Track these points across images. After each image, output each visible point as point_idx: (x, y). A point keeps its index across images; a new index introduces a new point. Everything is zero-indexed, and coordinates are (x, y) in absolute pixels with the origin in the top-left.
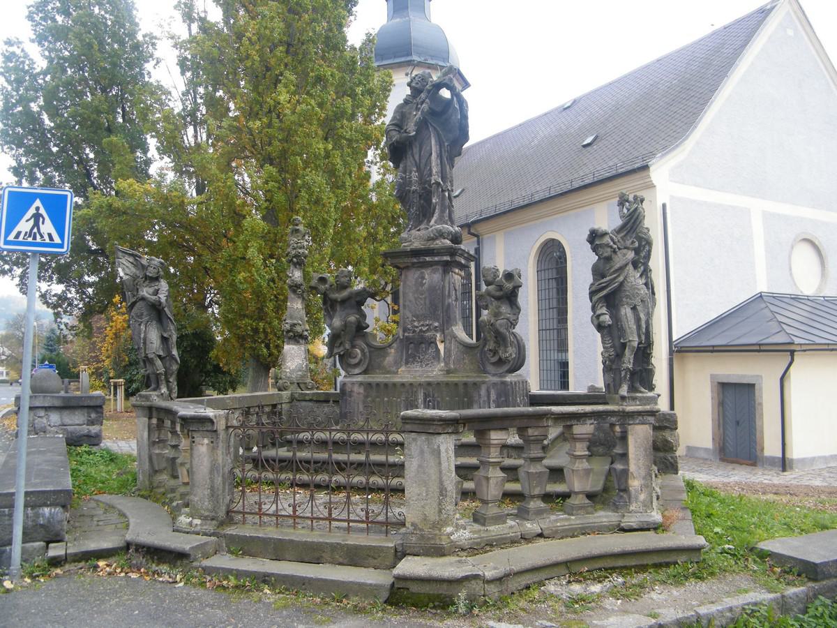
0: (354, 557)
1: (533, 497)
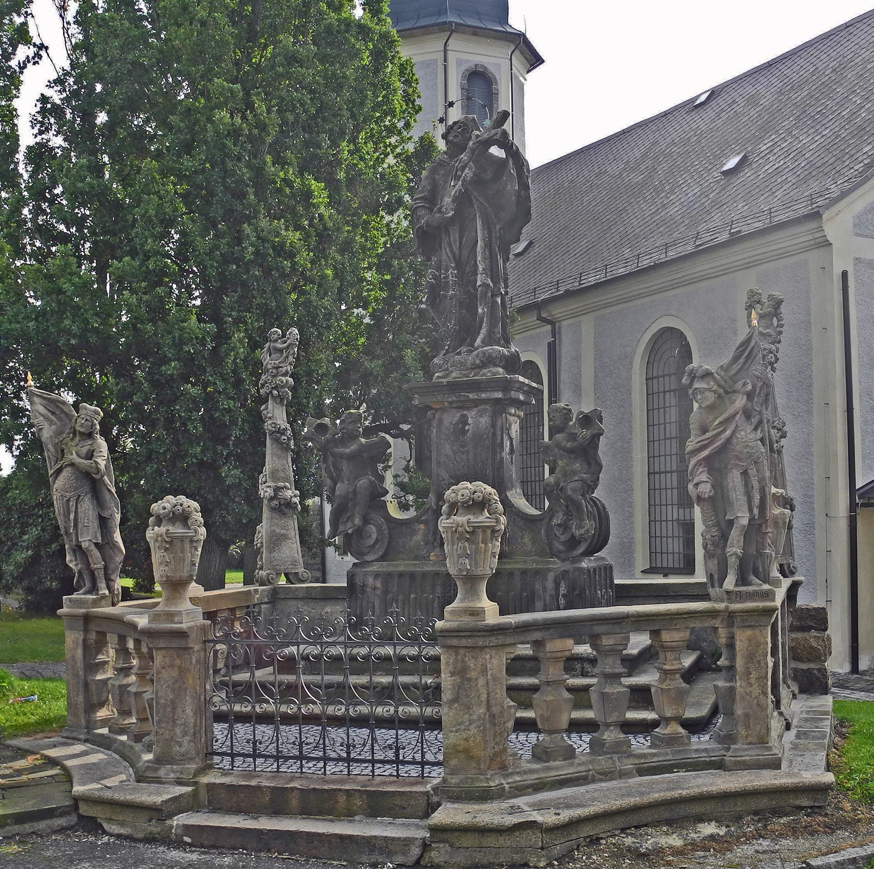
0: (378, 805)
1: (608, 725)
